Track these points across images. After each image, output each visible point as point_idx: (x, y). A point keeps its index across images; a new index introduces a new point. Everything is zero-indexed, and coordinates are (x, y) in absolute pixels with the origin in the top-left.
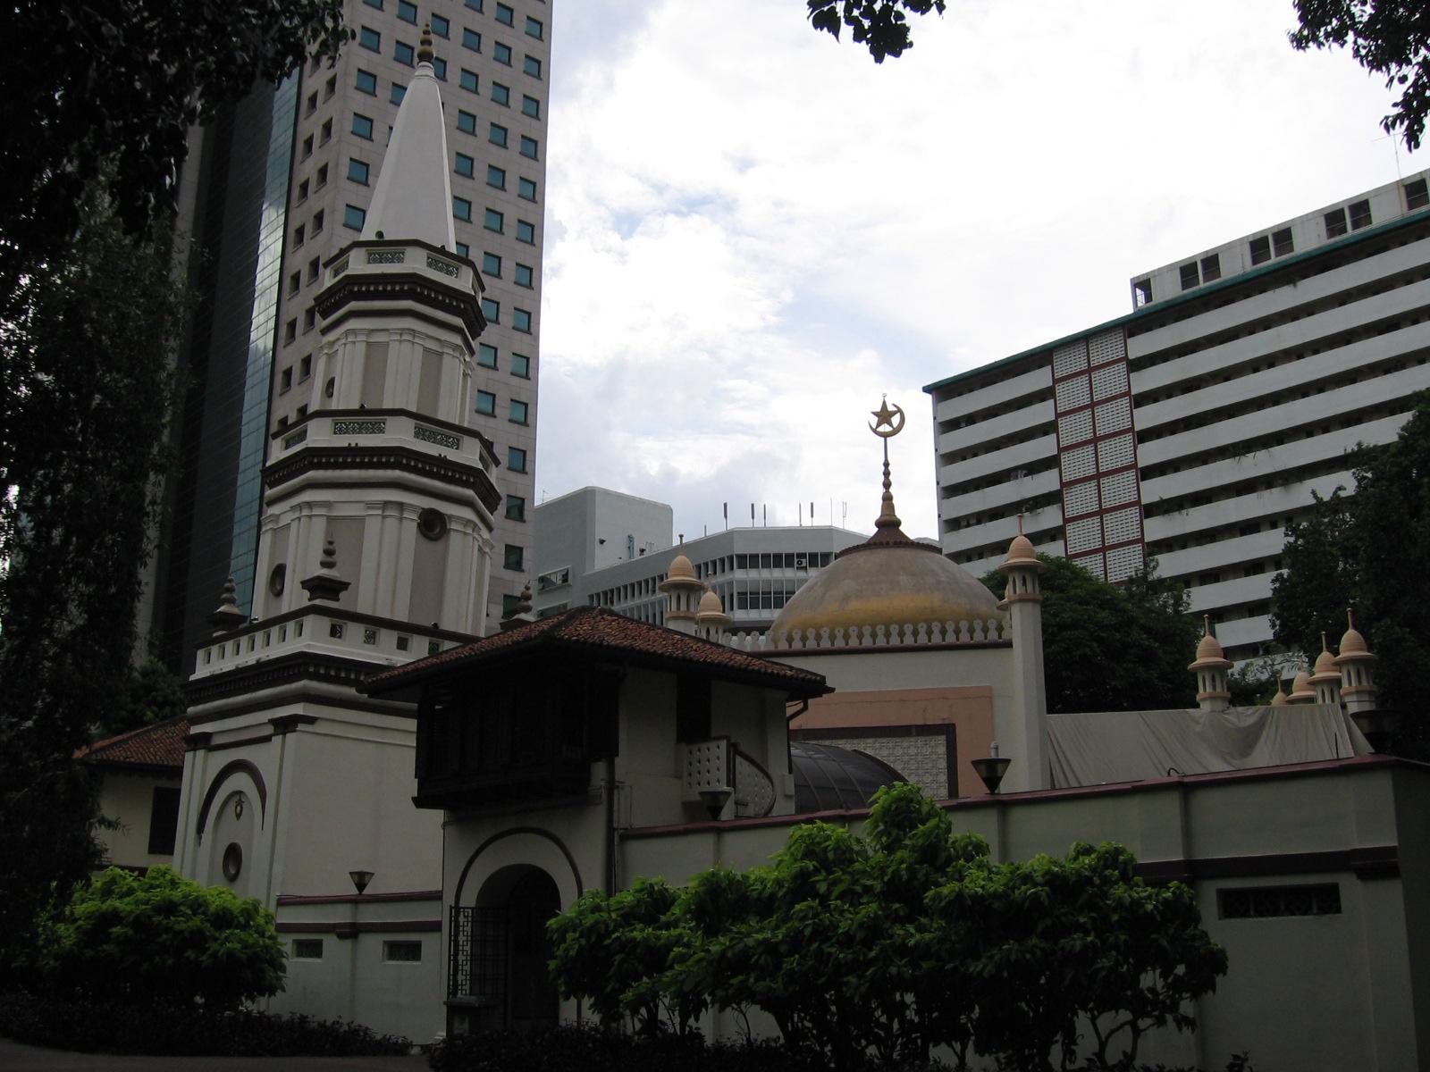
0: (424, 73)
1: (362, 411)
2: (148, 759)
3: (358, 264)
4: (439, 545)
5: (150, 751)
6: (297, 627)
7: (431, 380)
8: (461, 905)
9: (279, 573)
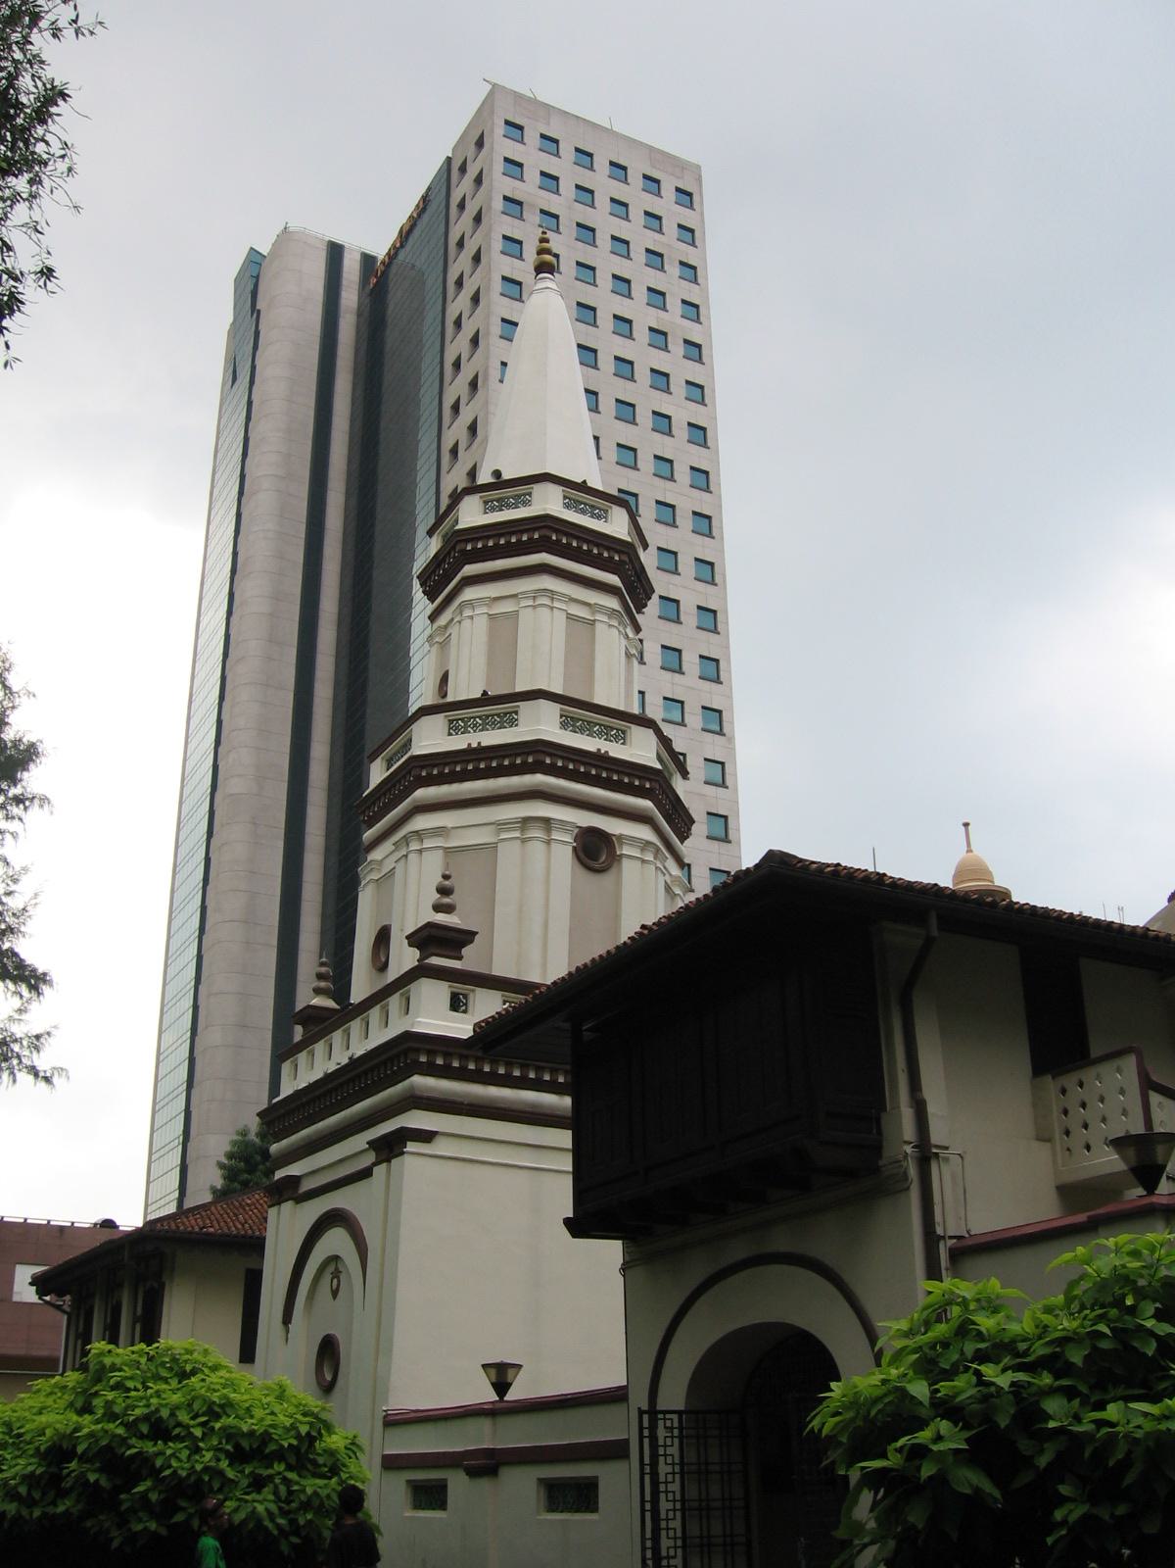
0: (544, 286)
1: (486, 700)
2: (233, 1229)
3: (472, 514)
4: (606, 880)
5: (238, 1219)
6: (404, 999)
7: (581, 654)
8: (659, 1408)
9: (383, 937)
